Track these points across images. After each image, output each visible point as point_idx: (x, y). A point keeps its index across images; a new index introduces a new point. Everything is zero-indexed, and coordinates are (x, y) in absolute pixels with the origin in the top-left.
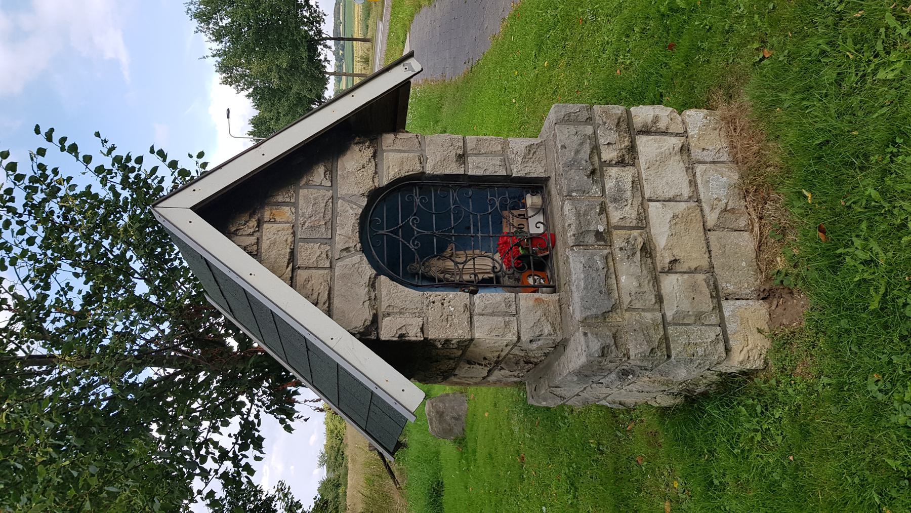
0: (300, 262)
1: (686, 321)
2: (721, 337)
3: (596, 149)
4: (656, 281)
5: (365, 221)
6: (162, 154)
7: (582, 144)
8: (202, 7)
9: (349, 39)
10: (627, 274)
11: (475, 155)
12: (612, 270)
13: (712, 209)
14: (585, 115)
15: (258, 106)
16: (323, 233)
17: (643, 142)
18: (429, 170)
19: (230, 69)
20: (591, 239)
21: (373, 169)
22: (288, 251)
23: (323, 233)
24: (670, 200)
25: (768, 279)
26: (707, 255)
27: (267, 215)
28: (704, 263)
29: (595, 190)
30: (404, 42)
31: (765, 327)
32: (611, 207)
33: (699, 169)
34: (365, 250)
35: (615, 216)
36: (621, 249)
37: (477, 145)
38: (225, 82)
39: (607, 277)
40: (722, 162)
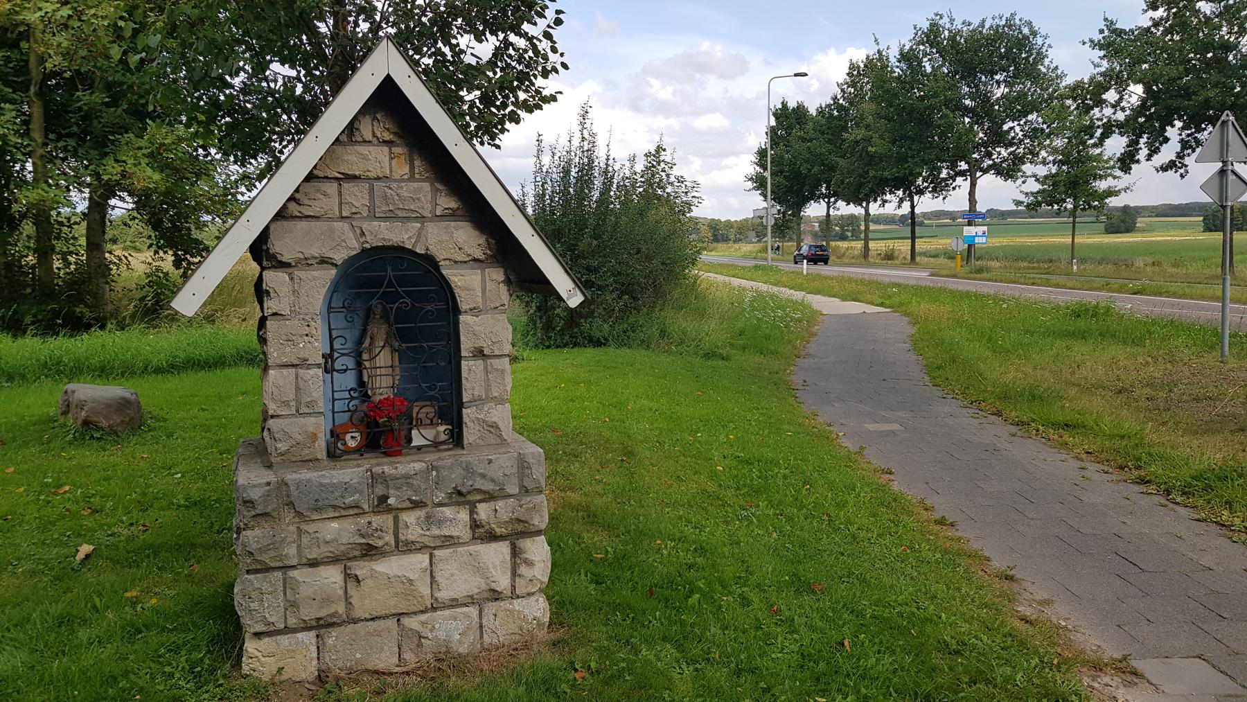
0: (345, 185)
1: (288, 591)
2: (272, 628)
3: (490, 497)
4: (334, 560)
5: (397, 253)
6: (558, 22)
7: (493, 481)
8: (946, 33)
9: (913, 232)
10: (340, 529)
11: (486, 368)
12: (343, 513)
13: (423, 623)
14: (529, 484)
15: (821, 112)
16: (381, 209)
17: (503, 548)
18: (462, 318)
19: (870, 74)
20: (380, 490)
21: (459, 259)
22: (357, 173)
23: (381, 209)
24: (432, 577)
25: (338, 679)
26: (368, 616)
27: (397, 150)
28: (358, 613)
29: (440, 496)
30: (882, 305)
31: (285, 677)
32: (421, 513)
33: (473, 611)
34: (364, 251)
35: (409, 518)
36: (370, 523)
37: (497, 370)
38: (853, 67)
39: (335, 507)
40: (482, 637)
